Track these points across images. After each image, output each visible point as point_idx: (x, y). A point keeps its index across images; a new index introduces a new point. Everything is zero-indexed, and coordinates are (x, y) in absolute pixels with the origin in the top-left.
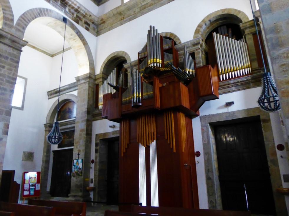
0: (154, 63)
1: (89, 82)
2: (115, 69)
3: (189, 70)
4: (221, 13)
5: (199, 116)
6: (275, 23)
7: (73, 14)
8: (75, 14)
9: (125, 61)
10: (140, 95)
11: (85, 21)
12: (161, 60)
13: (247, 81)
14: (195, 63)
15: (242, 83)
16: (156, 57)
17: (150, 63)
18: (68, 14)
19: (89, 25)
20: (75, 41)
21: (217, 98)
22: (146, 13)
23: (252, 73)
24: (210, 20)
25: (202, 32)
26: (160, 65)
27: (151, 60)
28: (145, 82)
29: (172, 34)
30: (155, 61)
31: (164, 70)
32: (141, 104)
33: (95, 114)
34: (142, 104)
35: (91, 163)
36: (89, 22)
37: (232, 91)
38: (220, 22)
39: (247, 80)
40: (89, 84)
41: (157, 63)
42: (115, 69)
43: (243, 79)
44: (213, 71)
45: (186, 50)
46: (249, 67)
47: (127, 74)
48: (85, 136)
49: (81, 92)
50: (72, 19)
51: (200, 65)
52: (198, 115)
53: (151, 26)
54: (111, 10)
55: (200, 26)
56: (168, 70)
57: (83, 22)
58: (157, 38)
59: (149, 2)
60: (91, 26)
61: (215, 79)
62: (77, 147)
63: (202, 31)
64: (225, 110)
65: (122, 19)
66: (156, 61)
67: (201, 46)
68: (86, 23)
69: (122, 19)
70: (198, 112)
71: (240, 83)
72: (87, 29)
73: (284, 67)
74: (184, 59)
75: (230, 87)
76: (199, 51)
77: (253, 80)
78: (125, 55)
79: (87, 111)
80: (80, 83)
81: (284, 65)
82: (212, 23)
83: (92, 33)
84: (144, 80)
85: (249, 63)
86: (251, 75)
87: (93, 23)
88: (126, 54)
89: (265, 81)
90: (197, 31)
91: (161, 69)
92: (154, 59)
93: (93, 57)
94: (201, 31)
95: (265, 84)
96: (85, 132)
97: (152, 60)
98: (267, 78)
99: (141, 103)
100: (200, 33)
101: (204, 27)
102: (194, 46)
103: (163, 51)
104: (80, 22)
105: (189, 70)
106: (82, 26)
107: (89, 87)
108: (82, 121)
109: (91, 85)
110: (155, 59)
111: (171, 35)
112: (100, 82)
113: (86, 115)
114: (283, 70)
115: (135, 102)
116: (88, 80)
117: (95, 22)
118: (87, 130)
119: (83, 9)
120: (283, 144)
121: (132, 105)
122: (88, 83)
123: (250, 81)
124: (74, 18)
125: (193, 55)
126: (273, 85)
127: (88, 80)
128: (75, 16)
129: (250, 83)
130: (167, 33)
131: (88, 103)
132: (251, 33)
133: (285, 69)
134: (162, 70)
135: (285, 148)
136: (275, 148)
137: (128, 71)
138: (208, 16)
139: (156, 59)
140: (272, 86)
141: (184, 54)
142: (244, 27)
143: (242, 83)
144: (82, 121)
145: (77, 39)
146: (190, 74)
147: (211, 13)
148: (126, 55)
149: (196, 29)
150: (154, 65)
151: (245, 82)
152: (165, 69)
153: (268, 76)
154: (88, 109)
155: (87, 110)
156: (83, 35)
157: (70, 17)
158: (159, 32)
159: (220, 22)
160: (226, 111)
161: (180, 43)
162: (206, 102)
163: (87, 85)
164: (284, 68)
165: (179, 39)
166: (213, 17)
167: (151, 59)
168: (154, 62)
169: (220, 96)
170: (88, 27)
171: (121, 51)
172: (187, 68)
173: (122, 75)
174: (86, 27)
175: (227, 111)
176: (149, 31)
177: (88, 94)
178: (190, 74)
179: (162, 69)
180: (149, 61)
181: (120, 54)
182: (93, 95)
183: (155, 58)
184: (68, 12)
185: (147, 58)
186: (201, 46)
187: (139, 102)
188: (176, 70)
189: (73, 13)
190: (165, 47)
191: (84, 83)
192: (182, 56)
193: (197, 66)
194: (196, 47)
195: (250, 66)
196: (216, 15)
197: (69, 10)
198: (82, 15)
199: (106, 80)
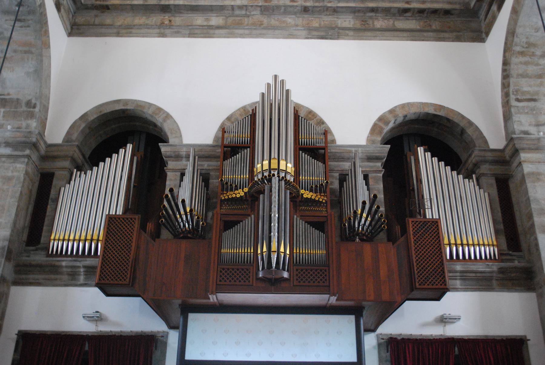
2: (130, 147)
4: (431, 111)
13: (488, 275)
15: (478, 275)
17: (259, 170)
32: (286, 275)
33: (31, 265)
38: (416, 126)
39: (489, 277)
43: (481, 267)
71: (474, 275)
77: (501, 275)
78: (164, 120)
92: (264, 163)
93: (51, 88)
97: (266, 163)
102: (368, 162)
107: (27, 173)
109: (30, 170)
111: (310, 116)
112: (63, 168)
123: (495, 275)
129: (492, 280)
132: (493, 175)
138: (403, 106)
142: (480, 159)
143: (478, 275)
145: (30, 22)
148: (168, 121)
149: (375, 125)
151: (483, 275)
155: (6, 243)
156: (47, 18)
159: (416, 126)
162: (407, 302)
166: (415, 113)
171: (150, 105)
175: (443, 334)
177: (18, 194)
180: (259, 166)
181: (145, 110)
182: (29, 203)
187: (284, 269)
191: (9, 156)
194: (371, 164)
196: (422, 111)
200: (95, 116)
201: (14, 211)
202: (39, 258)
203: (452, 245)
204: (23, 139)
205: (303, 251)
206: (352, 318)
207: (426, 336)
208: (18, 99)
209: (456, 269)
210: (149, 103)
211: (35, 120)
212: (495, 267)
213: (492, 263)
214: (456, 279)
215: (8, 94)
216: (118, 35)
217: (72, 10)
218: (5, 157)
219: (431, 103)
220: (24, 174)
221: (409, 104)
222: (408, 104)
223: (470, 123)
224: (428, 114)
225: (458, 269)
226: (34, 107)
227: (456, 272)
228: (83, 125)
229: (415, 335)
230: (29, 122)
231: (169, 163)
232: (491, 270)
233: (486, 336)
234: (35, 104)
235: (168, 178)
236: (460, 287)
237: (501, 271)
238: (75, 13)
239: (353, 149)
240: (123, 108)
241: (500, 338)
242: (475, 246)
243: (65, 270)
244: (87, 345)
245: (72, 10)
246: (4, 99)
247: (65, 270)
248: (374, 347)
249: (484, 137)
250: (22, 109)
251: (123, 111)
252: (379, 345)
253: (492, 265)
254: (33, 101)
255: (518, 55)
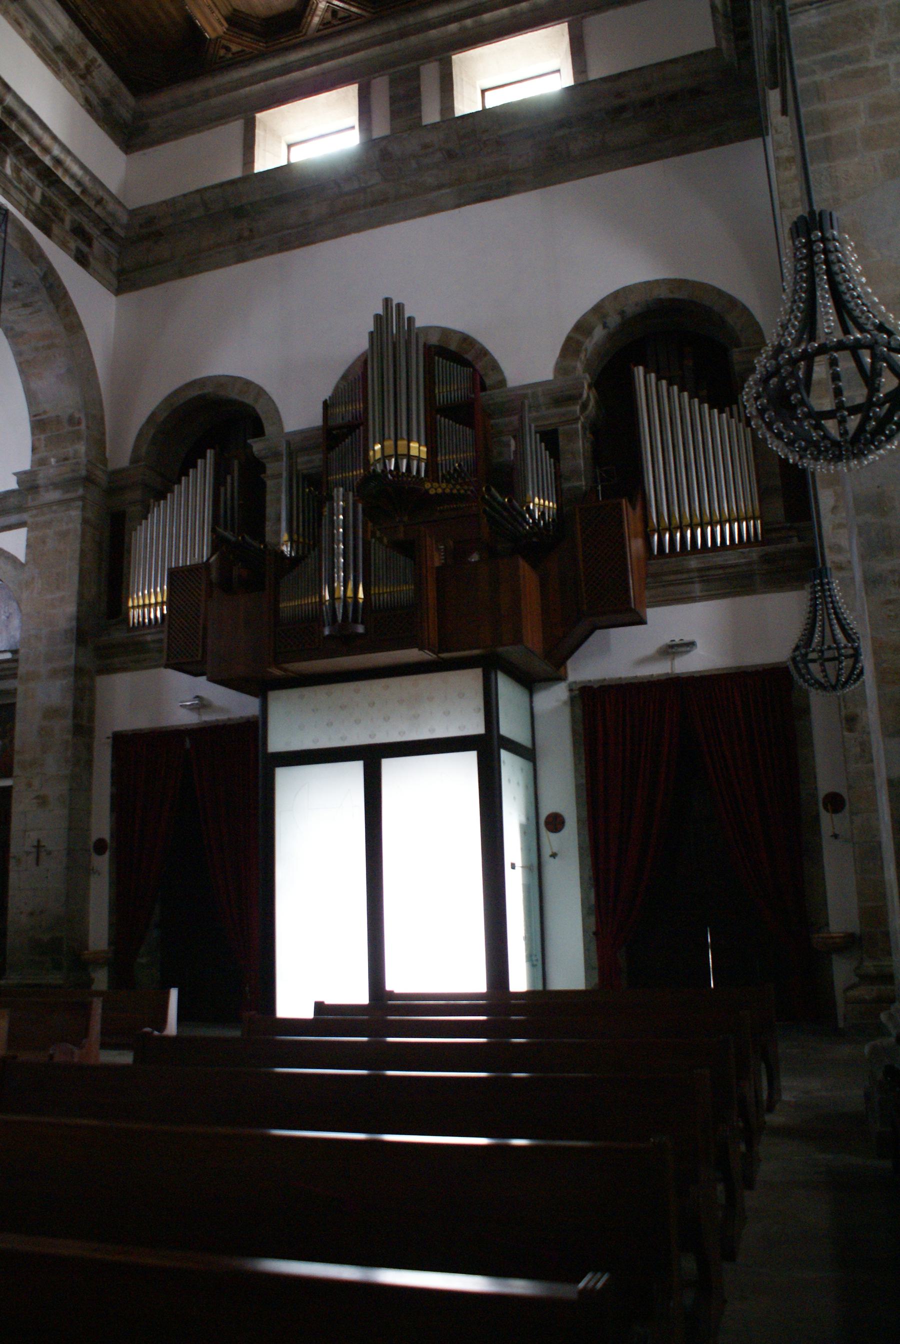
0: (398, 457)
1: (82, 498)
2: (210, 453)
3: (536, 500)
5: (570, 685)
6: (878, 487)
7: (31, 190)
8: (37, 188)
9: (258, 430)
10: (361, 595)
11: (73, 221)
12: (426, 445)
14: (558, 476)
16: (405, 435)
17: (378, 456)
18: (13, 191)
19: (88, 240)
20: (30, 310)
21: (642, 621)
22: (358, 229)
23: (763, 543)
24: (622, 313)
25: (589, 352)
26: (423, 465)
27: (386, 443)
28: (380, 540)
29: (467, 340)
30: (402, 450)
31: (440, 491)
32: (361, 629)
34: (366, 629)
35: (94, 855)
36: (89, 227)
37: (693, 599)
40: (84, 509)
41: (409, 457)
42: (208, 455)
43: (732, 558)
44: (631, 518)
45: (527, 417)
46: (755, 519)
47: (264, 484)
48: (69, 737)
49: (44, 542)
50: (26, 215)
51: (577, 484)
52: (562, 678)
53: (387, 302)
54: (197, 191)
55: (582, 328)
56: (455, 491)
57: (67, 225)
58: (414, 346)
59: (372, 186)
60: (96, 244)
61: (636, 546)
62: (29, 785)
63: (590, 349)
64: (660, 669)
65: (246, 234)
66: (405, 452)
67: (584, 407)
68: (78, 231)
69: (246, 234)
70: (562, 669)
71: (721, 572)
72: (82, 260)
73: (891, 607)
74: (520, 452)
75: (682, 583)
76: (577, 429)
79: (78, 628)
80: (36, 503)
81: (889, 602)
82: (628, 323)
83: (102, 280)
84: (373, 535)
85: (757, 506)
86: (758, 546)
87: (108, 232)
88: (260, 392)
89: (816, 592)
90: (571, 347)
91: (427, 485)
92: (400, 443)
94: (586, 350)
95: (817, 605)
96: (68, 722)
98: (822, 584)
99: (362, 623)
100: (582, 356)
101: (599, 333)
103: (433, 410)
104: (56, 230)
105: (536, 500)
106: (63, 245)
107: (85, 521)
108: (54, 674)
110: (402, 443)
113: (73, 646)
114: (889, 616)
115: (340, 618)
116: (81, 491)
117: (117, 229)
118: (76, 714)
119: (75, 169)
120: (549, 833)
121: (327, 632)
122: (80, 503)
124: (33, 208)
125: (550, 438)
126: (843, 614)
127: (81, 491)
128: (37, 197)
130: (445, 332)
131: (81, 595)
133: (892, 614)
134: (432, 492)
135: (847, 807)
136: (817, 804)
137: (269, 472)
138: (616, 295)
139: (405, 442)
140: (836, 613)
141: (519, 436)
144: (54, 674)
145: (40, 303)
146: (544, 521)
147: (628, 284)
149: (569, 339)
150: (397, 466)
152: (444, 490)
153: (827, 578)
154: (78, 619)
155: (74, 623)
156: (64, 288)
157: (18, 205)
158: (420, 323)
160: (666, 672)
161: (502, 382)
163: (76, 514)
164: (890, 611)
165: (495, 366)
167: (384, 439)
168: (399, 452)
169: (653, 614)
170: (86, 249)
172: (531, 493)
173: (233, 478)
174: (78, 250)
175: (670, 671)
176: (377, 318)
177: (77, 555)
178: (544, 521)
179: (433, 488)
180: (378, 447)
183: (402, 439)
184: (10, 182)
185: (366, 431)
186: (584, 407)
187: (355, 621)
188: (503, 505)
189: (30, 184)
190: (445, 393)
191: (60, 502)
192: (504, 439)
193: (566, 485)
194: (561, 410)
195: (757, 513)
197: (17, 170)
198: (67, 192)
199: (165, 498)
200: (165, 414)
201: (75, 579)
202: (118, 635)
203: (684, 528)
204: (70, 475)
205: (384, 592)
206: (478, 672)
207: (645, 677)
208: (58, 416)
209: (690, 567)
210: (232, 377)
211: (82, 443)
212: (754, 554)
213: (748, 549)
214: (693, 583)
215: (45, 412)
216: (182, 274)
217: (113, 251)
218: (56, 505)
219: (664, 280)
220: (81, 524)
221: (626, 291)
222: (624, 289)
223: (733, 302)
224: (660, 301)
225: (693, 566)
226: (79, 423)
227: (689, 571)
228: (152, 431)
229: (626, 678)
230: (77, 446)
231: (268, 465)
232: (748, 560)
233: (739, 668)
234: (80, 418)
235: (268, 490)
236: (698, 594)
237: (766, 559)
238: (120, 253)
239: (529, 391)
240: (200, 393)
241: (665, 677)
242: (705, 526)
243: (152, 645)
244: (188, 741)
245: (113, 251)
246: (42, 420)
247: (152, 645)
248: (565, 703)
249: (757, 323)
250: (65, 430)
251: (202, 397)
252: (572, 700)
253: (749, 552)
254: (77, 415)
255: (788, 165)
